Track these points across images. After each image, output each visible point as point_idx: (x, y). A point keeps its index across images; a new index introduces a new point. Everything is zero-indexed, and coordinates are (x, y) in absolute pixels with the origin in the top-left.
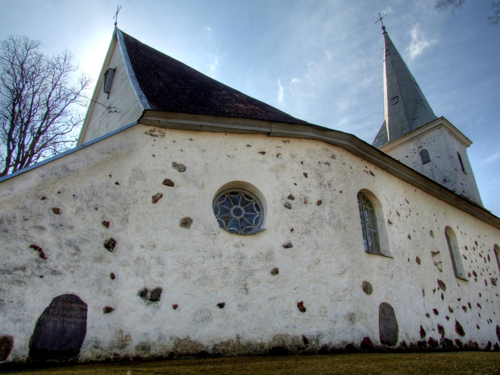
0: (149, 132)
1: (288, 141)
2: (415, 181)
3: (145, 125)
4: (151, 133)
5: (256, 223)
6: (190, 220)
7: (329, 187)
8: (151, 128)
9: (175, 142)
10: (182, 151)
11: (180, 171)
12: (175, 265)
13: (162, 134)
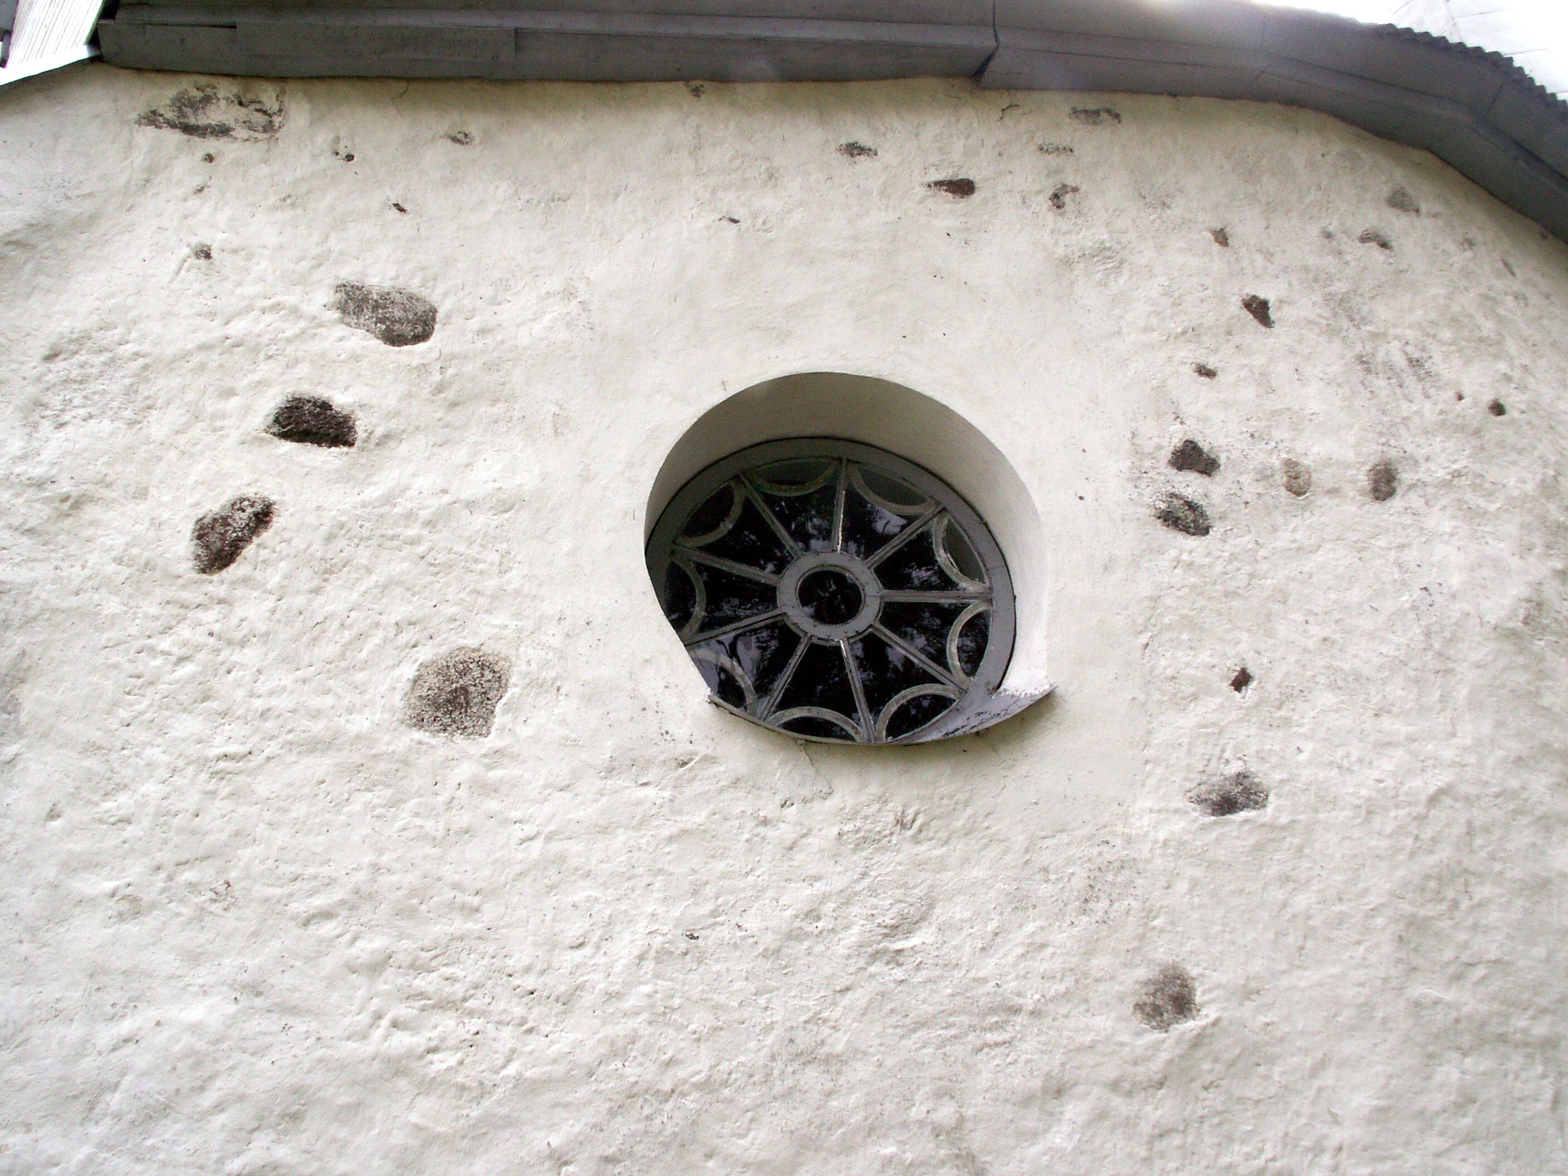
0: (170, 115)
1: (1108, 111)
2: (436, 957)
3: (139, 70)
4: (182, 114)
5: (973, 659)
6: (488, 676)
7: (1420, 379)
8: (187, 86)
9: (350, 158)
10: (402, 210)
11: (393, 339)
12: (395, 1024)
13: (259, 115)
